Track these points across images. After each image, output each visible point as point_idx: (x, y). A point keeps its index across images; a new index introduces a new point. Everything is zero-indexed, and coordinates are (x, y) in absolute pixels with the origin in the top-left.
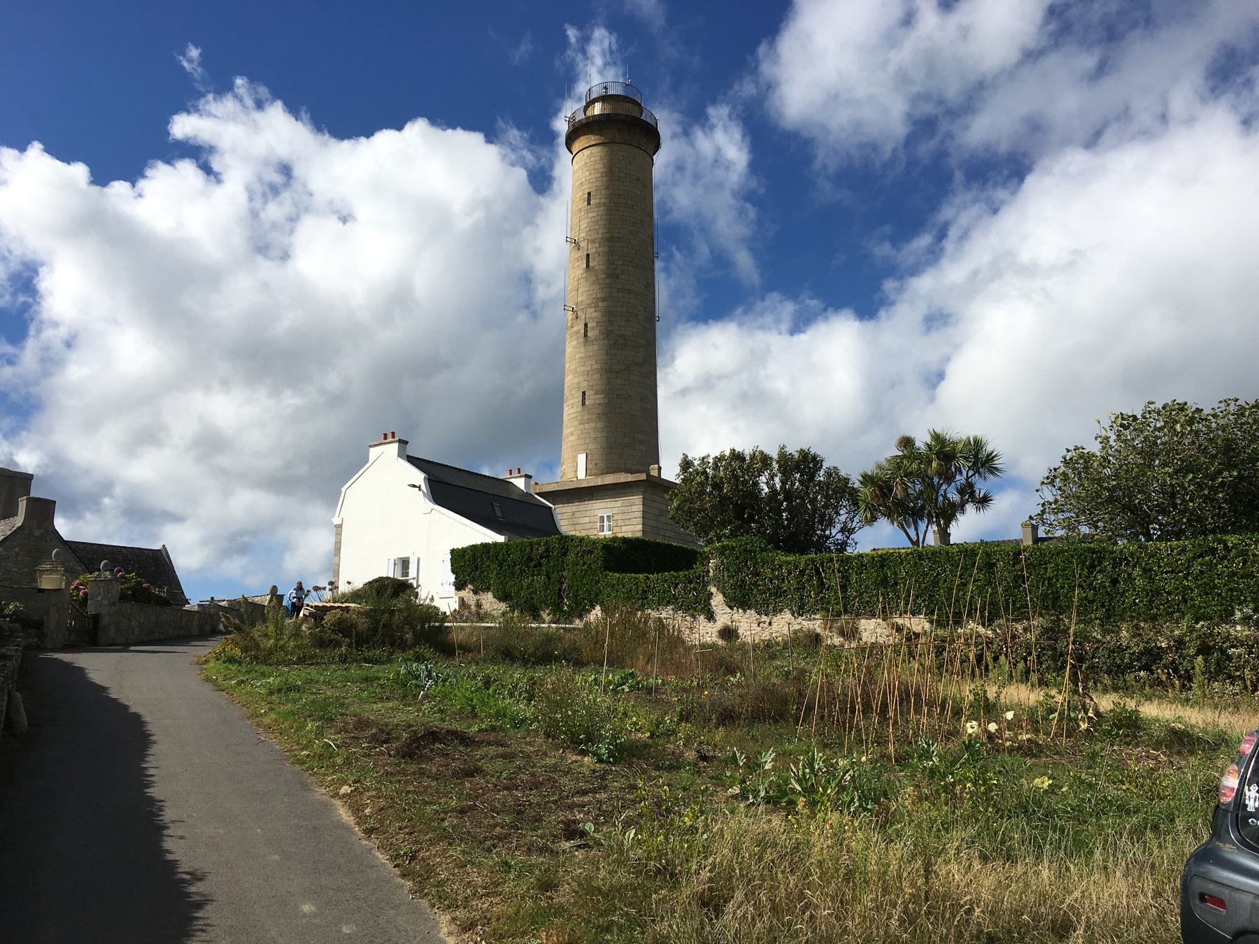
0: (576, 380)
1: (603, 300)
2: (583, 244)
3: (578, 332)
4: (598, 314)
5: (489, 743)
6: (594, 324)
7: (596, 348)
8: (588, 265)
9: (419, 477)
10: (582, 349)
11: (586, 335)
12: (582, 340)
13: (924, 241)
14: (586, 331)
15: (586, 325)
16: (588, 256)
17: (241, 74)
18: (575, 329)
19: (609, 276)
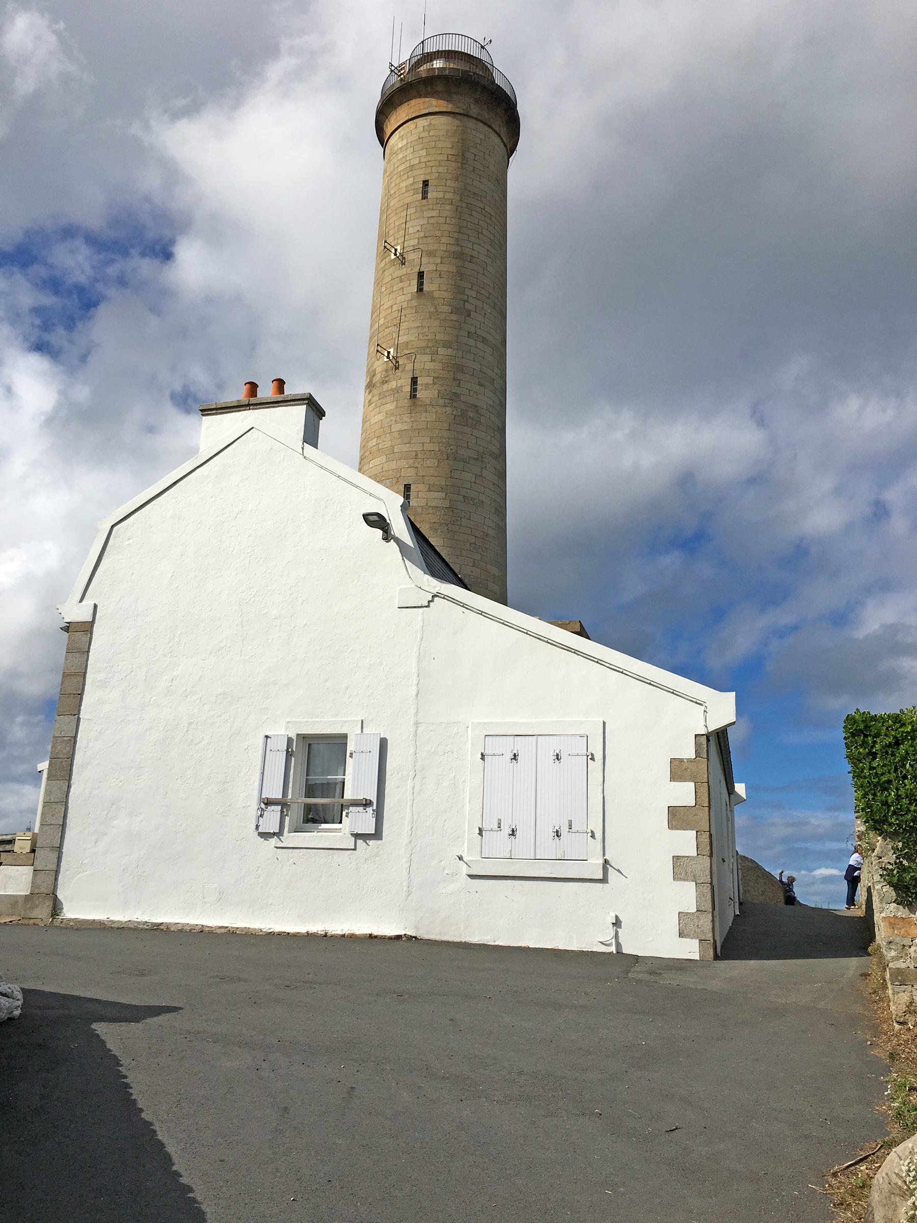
0: (393, 465)
1: (447, 345)
2: (411, 257)
3: (398, 390)
4: (437, 366)
5: (640, 972)
6: (430, 380)
7: (431, 417)
8: (420, 289)
9: (511, 159)
10: (406, 418)
11: (413, 396)
12: (406, 402)
13: (186, 928)
14: (414, 390)
15: (414, 381)
16: (421, 275)
17: (25, 1)
18: (393, 384)
19: (456, 310)
